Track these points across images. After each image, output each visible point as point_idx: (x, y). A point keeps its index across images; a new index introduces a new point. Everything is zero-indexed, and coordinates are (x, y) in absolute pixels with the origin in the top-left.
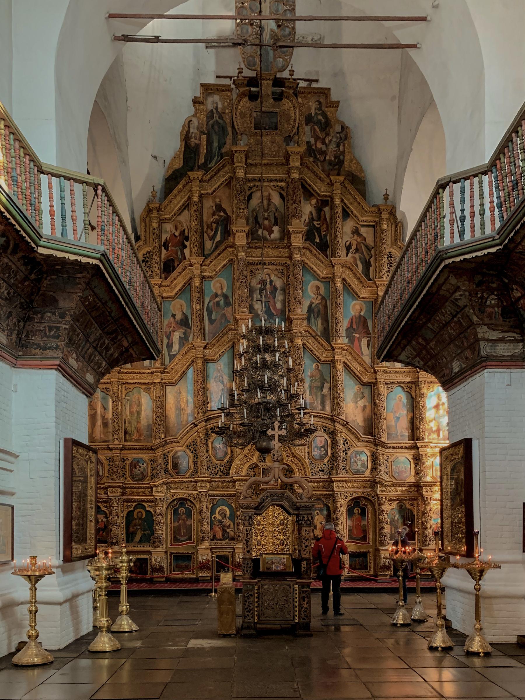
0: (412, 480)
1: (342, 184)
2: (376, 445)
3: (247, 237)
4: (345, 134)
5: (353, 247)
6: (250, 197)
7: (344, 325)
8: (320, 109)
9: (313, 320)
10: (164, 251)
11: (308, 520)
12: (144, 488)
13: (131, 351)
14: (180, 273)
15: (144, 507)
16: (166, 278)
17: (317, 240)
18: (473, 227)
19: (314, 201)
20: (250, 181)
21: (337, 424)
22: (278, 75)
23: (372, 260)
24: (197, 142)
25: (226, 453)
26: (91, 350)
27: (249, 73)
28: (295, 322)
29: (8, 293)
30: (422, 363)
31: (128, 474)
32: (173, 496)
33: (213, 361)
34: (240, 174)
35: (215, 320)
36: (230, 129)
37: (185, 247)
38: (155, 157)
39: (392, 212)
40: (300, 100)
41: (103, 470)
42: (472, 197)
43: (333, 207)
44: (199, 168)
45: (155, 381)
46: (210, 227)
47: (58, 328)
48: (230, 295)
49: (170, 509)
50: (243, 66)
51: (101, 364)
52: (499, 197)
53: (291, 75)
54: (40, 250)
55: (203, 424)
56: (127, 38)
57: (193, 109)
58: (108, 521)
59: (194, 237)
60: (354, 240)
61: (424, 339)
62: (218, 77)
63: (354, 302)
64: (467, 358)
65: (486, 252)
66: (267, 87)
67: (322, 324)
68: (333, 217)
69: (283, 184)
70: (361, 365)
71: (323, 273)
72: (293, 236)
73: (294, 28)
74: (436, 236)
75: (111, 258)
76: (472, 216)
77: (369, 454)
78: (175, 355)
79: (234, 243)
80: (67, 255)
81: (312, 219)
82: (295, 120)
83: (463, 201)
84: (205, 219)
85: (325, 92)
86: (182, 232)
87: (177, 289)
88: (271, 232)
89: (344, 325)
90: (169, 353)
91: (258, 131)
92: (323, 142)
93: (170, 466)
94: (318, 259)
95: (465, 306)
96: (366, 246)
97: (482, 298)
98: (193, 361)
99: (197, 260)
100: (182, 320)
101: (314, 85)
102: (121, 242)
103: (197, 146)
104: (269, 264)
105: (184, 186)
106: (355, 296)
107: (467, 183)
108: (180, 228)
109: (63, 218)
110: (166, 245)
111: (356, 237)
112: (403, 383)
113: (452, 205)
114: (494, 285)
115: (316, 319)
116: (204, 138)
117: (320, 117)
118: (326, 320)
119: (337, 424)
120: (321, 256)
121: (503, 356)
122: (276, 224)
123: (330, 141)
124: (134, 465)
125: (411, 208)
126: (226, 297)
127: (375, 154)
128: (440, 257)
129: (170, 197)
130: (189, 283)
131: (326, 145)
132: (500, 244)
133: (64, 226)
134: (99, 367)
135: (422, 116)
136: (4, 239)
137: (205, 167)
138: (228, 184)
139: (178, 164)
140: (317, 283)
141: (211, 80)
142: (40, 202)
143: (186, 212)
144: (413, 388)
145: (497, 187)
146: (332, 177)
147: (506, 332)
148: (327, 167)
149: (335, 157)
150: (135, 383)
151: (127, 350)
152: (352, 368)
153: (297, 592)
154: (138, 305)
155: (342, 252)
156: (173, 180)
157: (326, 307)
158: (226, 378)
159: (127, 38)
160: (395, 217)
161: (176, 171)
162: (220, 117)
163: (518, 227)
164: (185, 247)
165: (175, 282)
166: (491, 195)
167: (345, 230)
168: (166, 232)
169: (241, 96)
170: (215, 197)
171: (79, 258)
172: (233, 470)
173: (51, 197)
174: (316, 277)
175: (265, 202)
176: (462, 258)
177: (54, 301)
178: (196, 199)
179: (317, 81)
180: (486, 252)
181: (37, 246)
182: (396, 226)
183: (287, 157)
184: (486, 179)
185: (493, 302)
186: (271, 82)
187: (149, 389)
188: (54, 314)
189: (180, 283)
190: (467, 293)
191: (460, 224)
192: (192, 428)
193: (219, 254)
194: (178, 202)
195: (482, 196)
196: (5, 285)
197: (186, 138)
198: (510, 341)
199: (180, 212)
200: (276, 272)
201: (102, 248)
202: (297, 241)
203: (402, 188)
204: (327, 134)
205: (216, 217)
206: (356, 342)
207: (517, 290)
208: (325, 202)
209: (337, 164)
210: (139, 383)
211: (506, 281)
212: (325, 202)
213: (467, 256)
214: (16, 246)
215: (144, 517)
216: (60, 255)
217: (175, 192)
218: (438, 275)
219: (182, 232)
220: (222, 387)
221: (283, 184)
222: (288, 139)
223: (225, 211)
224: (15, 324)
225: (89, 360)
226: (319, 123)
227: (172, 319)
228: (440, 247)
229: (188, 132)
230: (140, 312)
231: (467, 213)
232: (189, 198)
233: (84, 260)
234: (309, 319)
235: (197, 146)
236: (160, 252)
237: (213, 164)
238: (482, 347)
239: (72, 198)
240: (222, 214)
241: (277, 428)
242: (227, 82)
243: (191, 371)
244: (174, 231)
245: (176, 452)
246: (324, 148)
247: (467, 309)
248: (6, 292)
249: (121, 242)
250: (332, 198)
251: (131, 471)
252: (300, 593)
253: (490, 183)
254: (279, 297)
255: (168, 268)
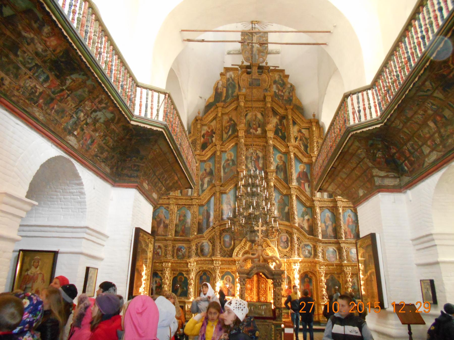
0: (337, 262)
1: (292, 109)
2: (316, 241)
3: (245, 132)
4: (292, 88)
5: (299, 138)
6: (246, 115)
7: (295, 176)
8: (280, 78)
9: (279, 172)
10: (202, 139)
11: (279, 282)
12: (183, 263)
13: (179, 182)
14: (210, 149)
15: (183, 275)
16: (202, 151)
17: (280, 135)
18: (365, 115)
19: (278, 117)
20: (246, 108)
21: (293, 229)
22: (261, 65)
23: (308, 145)
24: (221, 91)
25: (231, 244)
26: (156, 180)
27: (246, 64)
28: (269, 174)
29: (113, 145)
30: (340, 192)
31: (175, 255)
32: (200, 268)
33: (225, 193)
34: (242, 104)
35: (227, 172)
36: (237, 86)
37: (213, 137)
38: (201, 97)
39: (317, 122)
40: (271, 74)
41: (162, 252)
42: (363, 100)
43: (288, 120)
44: (222, 102)
45: (193, 203)
46: (226, 128)
47: (138, 166)
48: (235, 160)
49: (197, 276)
50: (244, 60)
51: (162, 188)
52: (378, 100)
53: (266, 64)
54: (132, 123)
55: (219, 227)
56: (189, 40)
57: (220, 77)
58: (162, 282)
59: (218, 132)
60: (299, 135)
61: (341, 178)
62: (232, 65)
63: (300, 164)
64: (367, 187)
65: (374, 127)
66: (255, 70)
67: (284, 175)
68: (288, 125)
69: (263, 109)
70: (305, 197)
71: (284, 150)
72: (268, 132)
73: (267, 47)
74: (345, 121)
75: (170, 129)
76: (365, 109)
77: (312, 246)
78: (204, 190)
79: (238, 135)
80: (146, 126)
81: (277, 125)
82: (268, 83)
83: (358, 103)
84: (224, 124)
85: (283, 71)
86: (212, 130)
87: (208, 156)
88: (257, 131)
89: (295, 176)
90: (202, 189)
91: (251, 87)
92: (282, 91)
93: (199, 251)
94: (281, 143)
95: (364, 158)
96: (306, 138)
97: (373, 153)
98: (214, 193)
99: (218, 143)
100: (209, 172)
101: (277, 68)
102: (177, 123)
103: (221, 93)
104: (256, 145)
105: (214, 110)
106: (300, 161)
107: (360, 94)
108: (211, 128)
109: (146, 107)
110: (203, 136)
111: (300, 134)
112: (329, 207)
113: (353, 104)
114: (380, 146)
115: (280, 172)
116: (225, 89)
117: (280, 81)
118: (285, 173)
119: (293, 229)
120: (282, 142)
121: (389, 186)
122: (259, 127)
123: (286, 91)
124: (179, 250)
125: (326, 119)
126: (233, 161)
127: (307, 96)
128: (349, 130)
129: (207, 114)
130: (214, 154)
131: (284, 93)
132: (382, 123)
133: (146, 111)
134: (161, 190)
135: (330, 79)
136: (112, 115)
137: (225, 101)
138: (236, 109)
139: (212, 100)
140: (280, 155)
141: (230, 66)
142: (135, 100)
143: (214, 121)
144: (335, 210)
145: (377, 95)
146: (287, 107)
147: (389, 172)
148: (284, 102)
149: (288, 98)
150: (183, 205)
151: (177, 182)
152: (301, 198)
153: (273, 330)
154: (184, 157)
155: (293, 140)
156: (209, 107)
157: (285, 166)
158: (232, 203)
159: (189, 40)
160: (319, 124)
161: (211, 103)
162: (233, 80)
163: (392, 112)
164: (213, 137)
165: (207, 153)
166: (374, 99)
167: (294, 131)
168: (204, 130)
169: (243, 73)
170: (229, 115)
171: (152, 128)
172: (235, 254)
173: (141, 98)
174: (280, 152)
175: (254, 117)
176: (361, 131)
177: (138, 152)
178: (220, 115)
179: (278, 67)
180: (374, 127)
181: (131, 120)
182: (320, 129)
183: (265, 97)
184: (370, 92)
185: (380, 155)
186: (257, 67)
187: (190, 208)
188: (137, 158)
189: (209, 154)
190: (365, 150)
191: (358, 114)
192: (212, 230)
193: (230, 140)
194: (211, 117)
195: (369, 100)
196: (111, 140)
197: (216, 89)
198: (392, 177)
199: (212, 121)
200: (259, 149)
201: (165, 123)
202: (270, 134)
203: (321, 111)
204: (284, 88)
205: (229, 124)
206: (302, 185)
207: (393, 148)
208: (283, 117)
209: (290, 101)
210: (185, 205)
211: (387, 144)
212: (283, 117)
213: (364, 130)
214: (119, 120)
215: (183, 280)
216: (142, 125)
217: (210, 112)
218: (348, 141)
219: (212, 130)
220: (229, 207)
221: (263, 109)
222: (266, 90)
223: (234, 121)
224: (115, 163)
225: (155, 185)
226: (280, 84)
227: (204, 171)
228: (348, 125)
229: (217, 87)
230: (185, 161)
231: (361, 108)
232: (216, 115)
233: (155, 129)
234: (276, 173)
235: (221, 93)
236: (201, 138)
237: (229, 100)
238: (376, 180)
239: (152, 99)
240: (232, 122)
241: (260, 226)
242: (237, 67)
243: (213, 199)
244: (208, 129)
245: (203, 243)
246: (282, 94)
247: (365, 159)
248: (112, 145)
249: (177, 123)
250: (287, 115)
251: (177, 252)
252: (275, 331)
253: (373, 94)
254: (261, 161)
255: (204, 146)
